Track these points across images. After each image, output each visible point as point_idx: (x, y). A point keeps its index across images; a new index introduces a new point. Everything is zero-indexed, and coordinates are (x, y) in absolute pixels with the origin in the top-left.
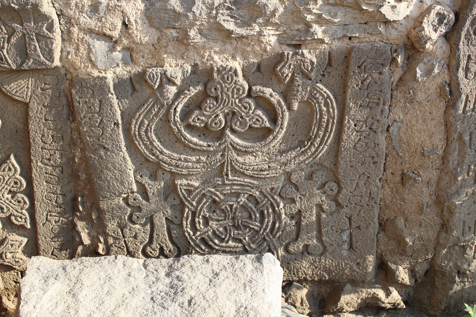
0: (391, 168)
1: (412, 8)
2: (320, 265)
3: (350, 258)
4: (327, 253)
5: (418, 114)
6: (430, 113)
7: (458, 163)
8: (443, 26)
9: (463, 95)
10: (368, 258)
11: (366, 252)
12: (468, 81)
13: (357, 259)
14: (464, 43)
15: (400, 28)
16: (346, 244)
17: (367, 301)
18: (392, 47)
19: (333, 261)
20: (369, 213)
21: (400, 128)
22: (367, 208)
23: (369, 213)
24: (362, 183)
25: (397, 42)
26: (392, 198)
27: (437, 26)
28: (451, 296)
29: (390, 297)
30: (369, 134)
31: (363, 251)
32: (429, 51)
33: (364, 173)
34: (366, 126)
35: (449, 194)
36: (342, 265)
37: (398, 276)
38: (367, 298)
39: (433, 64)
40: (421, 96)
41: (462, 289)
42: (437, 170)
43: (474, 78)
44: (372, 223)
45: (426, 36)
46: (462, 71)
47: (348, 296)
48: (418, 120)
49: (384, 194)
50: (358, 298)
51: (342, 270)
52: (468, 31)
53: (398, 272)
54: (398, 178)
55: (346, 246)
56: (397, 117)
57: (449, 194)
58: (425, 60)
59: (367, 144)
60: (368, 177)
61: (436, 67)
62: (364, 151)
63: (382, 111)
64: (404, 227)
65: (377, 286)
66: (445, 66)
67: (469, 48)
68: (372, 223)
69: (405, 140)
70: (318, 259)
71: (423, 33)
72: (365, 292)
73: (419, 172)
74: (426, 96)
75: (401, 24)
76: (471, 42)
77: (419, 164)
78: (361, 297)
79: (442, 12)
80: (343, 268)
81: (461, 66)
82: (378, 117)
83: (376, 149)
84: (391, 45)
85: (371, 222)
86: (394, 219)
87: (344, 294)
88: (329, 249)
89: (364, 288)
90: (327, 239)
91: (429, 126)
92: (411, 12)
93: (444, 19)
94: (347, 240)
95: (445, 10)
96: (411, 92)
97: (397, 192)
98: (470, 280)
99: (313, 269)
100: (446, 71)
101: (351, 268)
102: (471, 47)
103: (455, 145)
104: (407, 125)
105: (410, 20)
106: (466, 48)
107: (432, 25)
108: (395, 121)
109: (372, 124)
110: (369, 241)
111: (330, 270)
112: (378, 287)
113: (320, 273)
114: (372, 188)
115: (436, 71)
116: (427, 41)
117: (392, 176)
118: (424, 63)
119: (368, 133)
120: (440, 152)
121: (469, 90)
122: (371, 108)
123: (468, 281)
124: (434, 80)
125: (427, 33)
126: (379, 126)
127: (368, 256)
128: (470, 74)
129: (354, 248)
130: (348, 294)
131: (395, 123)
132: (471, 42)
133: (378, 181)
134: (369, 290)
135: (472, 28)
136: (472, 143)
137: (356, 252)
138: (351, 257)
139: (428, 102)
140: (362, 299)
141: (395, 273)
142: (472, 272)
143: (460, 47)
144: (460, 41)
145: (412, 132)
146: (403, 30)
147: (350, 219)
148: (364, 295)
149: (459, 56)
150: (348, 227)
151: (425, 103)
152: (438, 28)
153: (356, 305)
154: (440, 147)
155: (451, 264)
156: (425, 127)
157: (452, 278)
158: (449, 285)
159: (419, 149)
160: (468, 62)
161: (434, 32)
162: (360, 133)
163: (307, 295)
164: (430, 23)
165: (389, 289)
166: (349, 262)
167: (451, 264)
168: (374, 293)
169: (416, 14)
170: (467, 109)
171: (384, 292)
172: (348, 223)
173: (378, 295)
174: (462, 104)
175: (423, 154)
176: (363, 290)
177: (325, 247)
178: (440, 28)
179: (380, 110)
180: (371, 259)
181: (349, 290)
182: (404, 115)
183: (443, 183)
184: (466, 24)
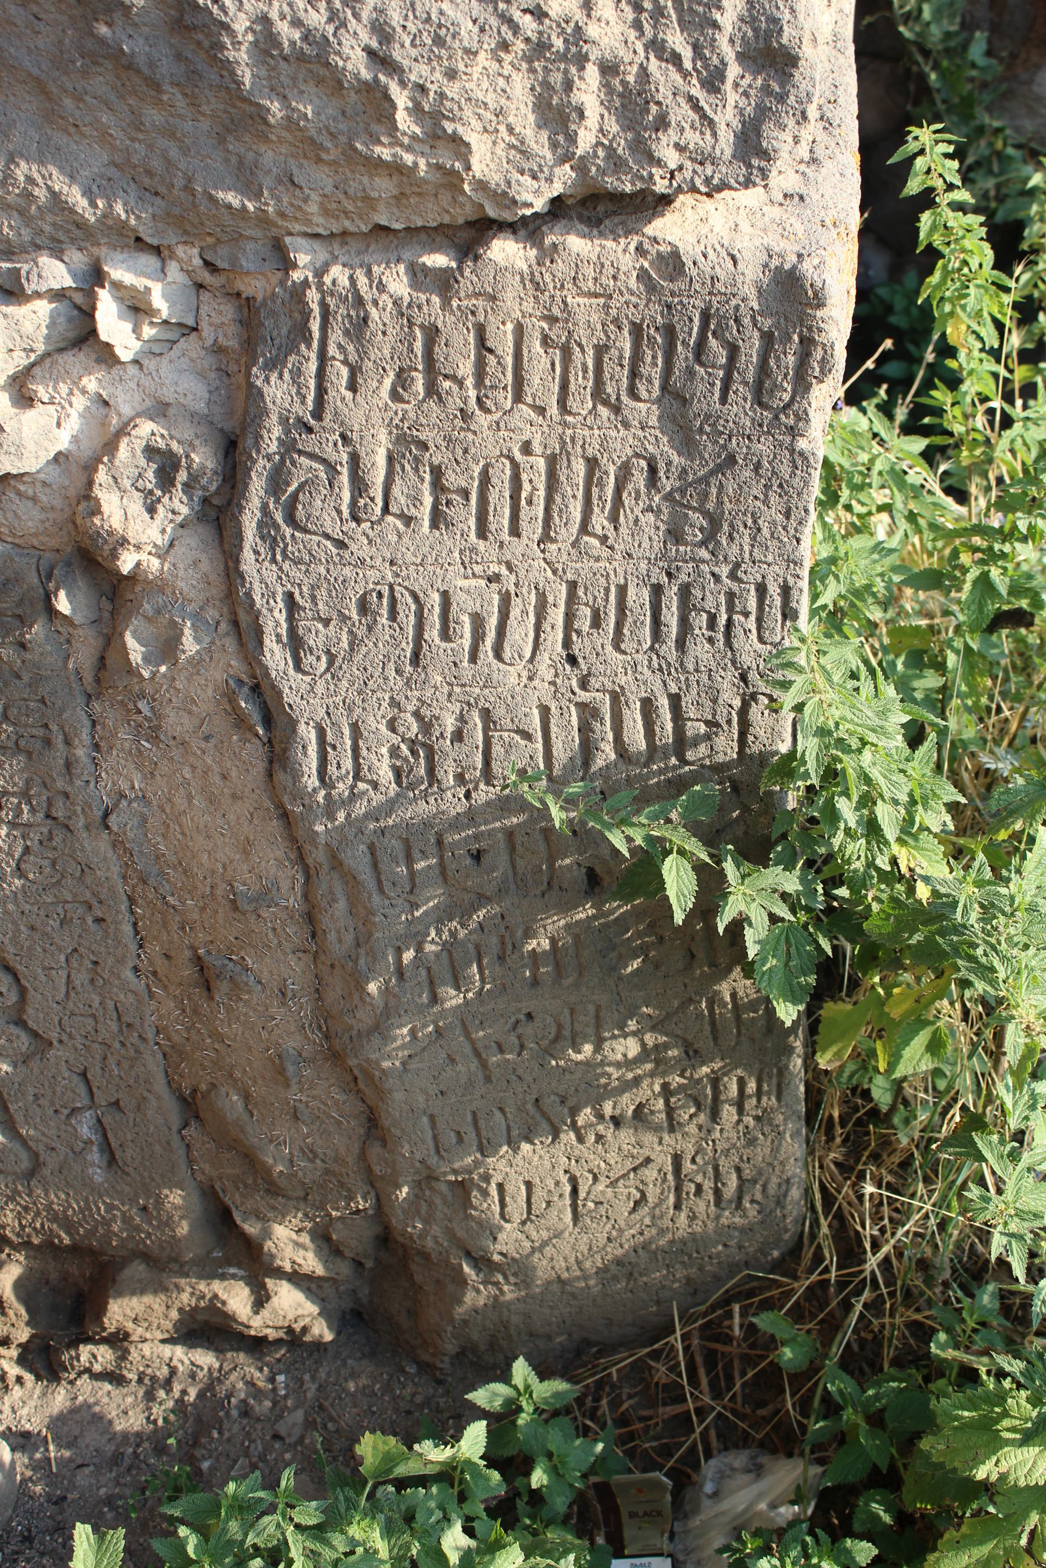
0: (156, 938)
1: (76, 427)
2: (35, 1203)
3: (117, 1192)
4: (46, 1172)
5: (187, 776)
6: (224, 777)
7: (357, 939)
8: (178, 492)
9: (302, 728)
10: (167, 1196)
11: (158, 1180)
12: (308, 679)
13: (137, 1196)
14: (257, 553)
15: (44, 499)
16: (95, 1148)
17: (199, 1317)
18: (40, 558)
19: (68, 1194)
20: (132, 1067)
21: (144, 820)
22: (123, 1051)
23: (132, 1067)
24: (81, 978)
25: (53, 543)
26: (188, 1029)
27: (159, 493)
28: (465, 1322)
29: (265, 1313)
30: (50, 832)
31: (146, 1174)
32: (151, 577)
33: (75, 950)
34: (33, 810)
35: (354, 1033)
36: (99, 1209)
37: (273, 1256)
38: (195, 1309)
39: (173, 624)
40: (177, 723)
41: (496, 1303)
42: (300, 954)
43: (328, 670)
44: (151, 1097)
45: (110, 533)
46: (277, 648)
47: (135, 1300)
48: (190, 797)
49: (161, 1017)
50: (168, 1307)
51: (102, 1224)
52: (265, 509)
53: (269, 1243)
54: (188, 972)
55: (95, 1156)
56: (124, 785)
57: (354, 1033)
58: (146, 606)
59: (54, 864)
60: (96, 963)
61: (187, 632)
62: (54, 885)
63: (68, 765)
64: (245, 1117)
65: (232, 1271)
66: (223, 626)
67: (281, 569)
68: (151, 1097)
69: (172, 859)
70: (23, 1185)
71: (97, 521)
72: (189, 1289)
73: (243, 958)
74: (196, 722)
75: (44, 484)
76: (284, 552)
77: (235, 933)
78: (178, 1304)
79: (161, 444)
80: (103, 1217)
81: (269, 628)
82: (60, 784)
83: (88, 880)
84: (37, 553)
85: (146, 1094)
86: (209, 1091)
87: (120, 1294)
88: (48, 1159)
89: (187, 1276)
90: (32, 1132)
91: (231, 817)
92: (75, 439)
93: (176, 467)
94: (93, 1138)
95: (172, 437)
96: (142, 705)
97: (195, 1011)
98: (512, 1279)
99: (19, 1213)
100: (230, 644)
101: (127, 1220)
102: (286, 566)
103: (328, 882)
104: (163, 811)
105: (74, 468)
106: (271, 573)
107: (137, 489)
108: (122, 796)
109: (50, 803)
110: (157, 1148)
111: (66, 1217)
112: (234, 1277)
113: (42, 1225)
114: (117, 994)
115: (190, 645)
116: (115, 549)
117: (166, 962)
118: (149, 619)
119: (45, 830)
120: (294, 901)
121: (322, 712)
122: (29, 754)
123: (508, 1283)
124: (198, 673)
125: (116, 522)
126: (75, 813)
127: (166, 1191)
128: (311, 659)
129: (120, 1163)
130: (133, 1293)
131: (124, 803)
132: (284, 552)
133: (129, 974)
134: (202, 1286)
135: (277, 501)
136: (383, 878)
137: (128, 1174)
138: (118, 1187)
139: (207, 738)
140: (180, 1310)
141: (261, 1247)
142: (513, 1259)
143: (244, 567)
144: (241, 549)
145: (183, 834)
146: (58, 503)
147: (84, 1075)
148: (185, 1298)
149: (249, 595)
150: (86, 1101)
151: (197, 744)
152: (159, 501)
153: (169, 1325)
154: (285, 885)
155: (436, 1230)
156: (220, 821)
157: (454, 1269)
158: (451, 1287)
159: (222, 889)
160: (291, 619)
161: (147, 516)
162: (21, 829)
163: (19, 1286)
164: (127, 483)
165: (264, 1286)
166: (116, 1203)
167: (436, 1230)
168: (216, 1296)
169: (87, 450)
170: (332, 769)
171: (252, 1292)
172: (82, 1090)
173: (224, 1303)
174: (305, 754)
175: (234, 905)
176: (183, 1282)
177: (36, 1155)
178: (166, 500)
179: (62, 762)
180: (178, 1201)
181: (140, 1281)
182: (145, 777)
183: (332, 996)
184: (252, 488)
